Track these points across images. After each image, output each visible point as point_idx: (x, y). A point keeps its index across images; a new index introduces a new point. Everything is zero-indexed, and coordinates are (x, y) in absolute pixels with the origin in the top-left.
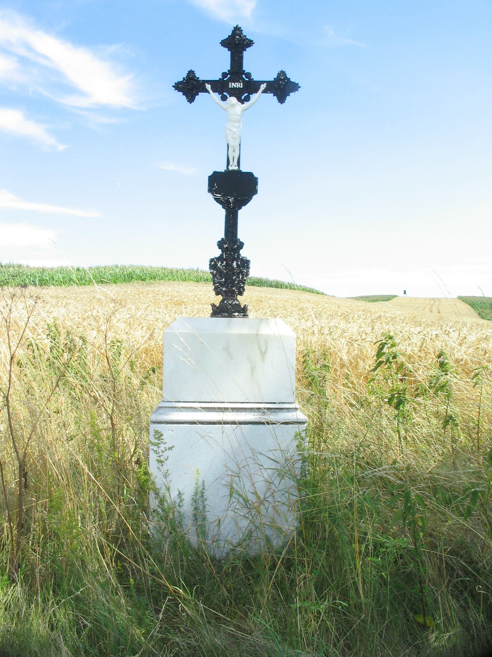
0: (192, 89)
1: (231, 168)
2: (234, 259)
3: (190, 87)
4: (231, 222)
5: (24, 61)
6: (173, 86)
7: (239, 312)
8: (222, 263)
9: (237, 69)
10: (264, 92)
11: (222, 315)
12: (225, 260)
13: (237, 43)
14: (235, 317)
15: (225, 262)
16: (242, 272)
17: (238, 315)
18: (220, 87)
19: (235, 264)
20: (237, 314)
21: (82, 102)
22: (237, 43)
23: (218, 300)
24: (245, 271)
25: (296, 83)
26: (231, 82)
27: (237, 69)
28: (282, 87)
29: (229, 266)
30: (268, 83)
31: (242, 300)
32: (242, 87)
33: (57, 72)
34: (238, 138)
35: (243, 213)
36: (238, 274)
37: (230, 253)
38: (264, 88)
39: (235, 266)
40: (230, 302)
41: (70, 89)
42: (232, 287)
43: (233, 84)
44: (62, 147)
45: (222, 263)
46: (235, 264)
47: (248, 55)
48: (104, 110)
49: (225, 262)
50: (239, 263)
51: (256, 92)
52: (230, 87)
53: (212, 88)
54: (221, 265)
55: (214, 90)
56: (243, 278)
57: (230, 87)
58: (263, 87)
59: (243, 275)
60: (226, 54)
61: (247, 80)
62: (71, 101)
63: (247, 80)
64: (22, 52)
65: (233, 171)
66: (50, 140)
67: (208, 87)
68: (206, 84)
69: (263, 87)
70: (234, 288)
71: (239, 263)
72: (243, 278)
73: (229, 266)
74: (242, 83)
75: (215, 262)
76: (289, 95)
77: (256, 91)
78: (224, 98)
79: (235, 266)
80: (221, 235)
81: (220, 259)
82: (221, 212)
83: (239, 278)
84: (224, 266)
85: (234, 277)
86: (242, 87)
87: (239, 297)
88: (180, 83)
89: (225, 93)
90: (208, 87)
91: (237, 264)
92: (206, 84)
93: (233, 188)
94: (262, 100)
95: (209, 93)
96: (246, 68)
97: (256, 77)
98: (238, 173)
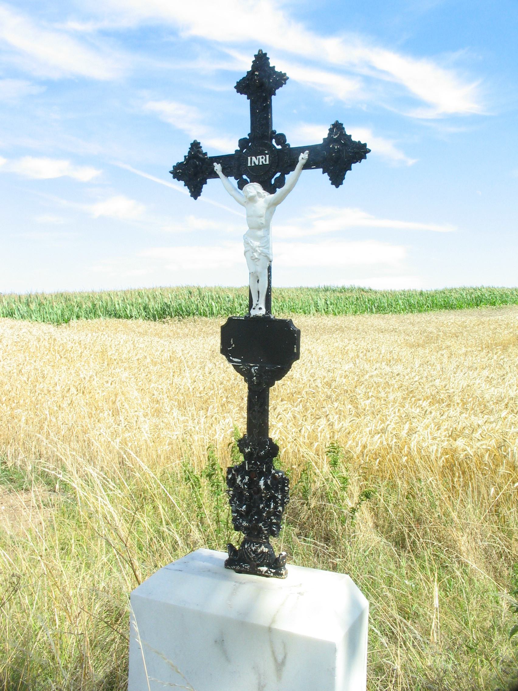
0: (196, 175)
1: (253, 313)
2: (261, 474)
3: (195, 170)
4: (256, 408)
5: (367, 80)
6: (170, 172)
7: (269, 566)
8: (243, 478)
9: (262, 131)
10: (306, 166)
11: (241, 566)
12: (248, 473)
13: (260, 84)
14: (260, 574)
15: (247, 478)
16: (274, 498)
17: (266, 572)
18: (234, 166)
19: (262, 483)
20: (264, 569)
21: (430, 114)
22: (260, 84)
23: (236, 537)
24: (280, 497)
25: (362, 142)
26: (251, 155)
27: (262, 131)
28: (339, 156)
29: (253, 484)
30: (312, 149)
31: (277, 545)
32: (267, 163)
33: (399, 87)
34: (261, 257)
35: (279, 391)
36: (269, 500)
37: (255, 464)
38: (304, 161)
39: (263, 487)
40: (253, 548)
41: (414, 102)
42: (258, 521)
43: (254, 158)
44: (411, 162)
45: (243, 478)
46: (262, 483)
47: (279, 101)
48: (454, 119)
49: (247, 478)
50: (269, 482)
51: (293, 170)
52: (249, 165)
53: (223, 171)
54: (241, 481)
55: (227, 173)
56: (276, 508)
57: (249, 165)
58: (303, 157)
59: (276, 503)
60: (243, 103)
61: (279, 147)
62: (416, 114)
63: (279, 147)
64: (366, 71)
65: (257, 318)
66: (399, 156)
67: (218, 167)
68: (215, 164)
69: (303, 157)
70: (261, 525)
71: (269, 482)
72: (276, 508)
73: (253, 484)
74: (267, 156)
75: (233, 474)
76: (350, 169)
77: (292, 167)
78: (242, 184)
79: (263, 487)
80: (242, 428)
81: (239, 470)
82: (241, 387)
83: (269, 506)
84: (245, 484)
85: (261, 506)
86: (267, 163)
87: (273, 541)
88: (179, 166)
89: (245, 177)
90: (218, 167)
91: (266, 484)
92: (215, 164)
93: (261, 345)
94: (309, 182)
95: (219, 177)
96: (278, 126)
97: (293, 142)
98: (266, 320)
